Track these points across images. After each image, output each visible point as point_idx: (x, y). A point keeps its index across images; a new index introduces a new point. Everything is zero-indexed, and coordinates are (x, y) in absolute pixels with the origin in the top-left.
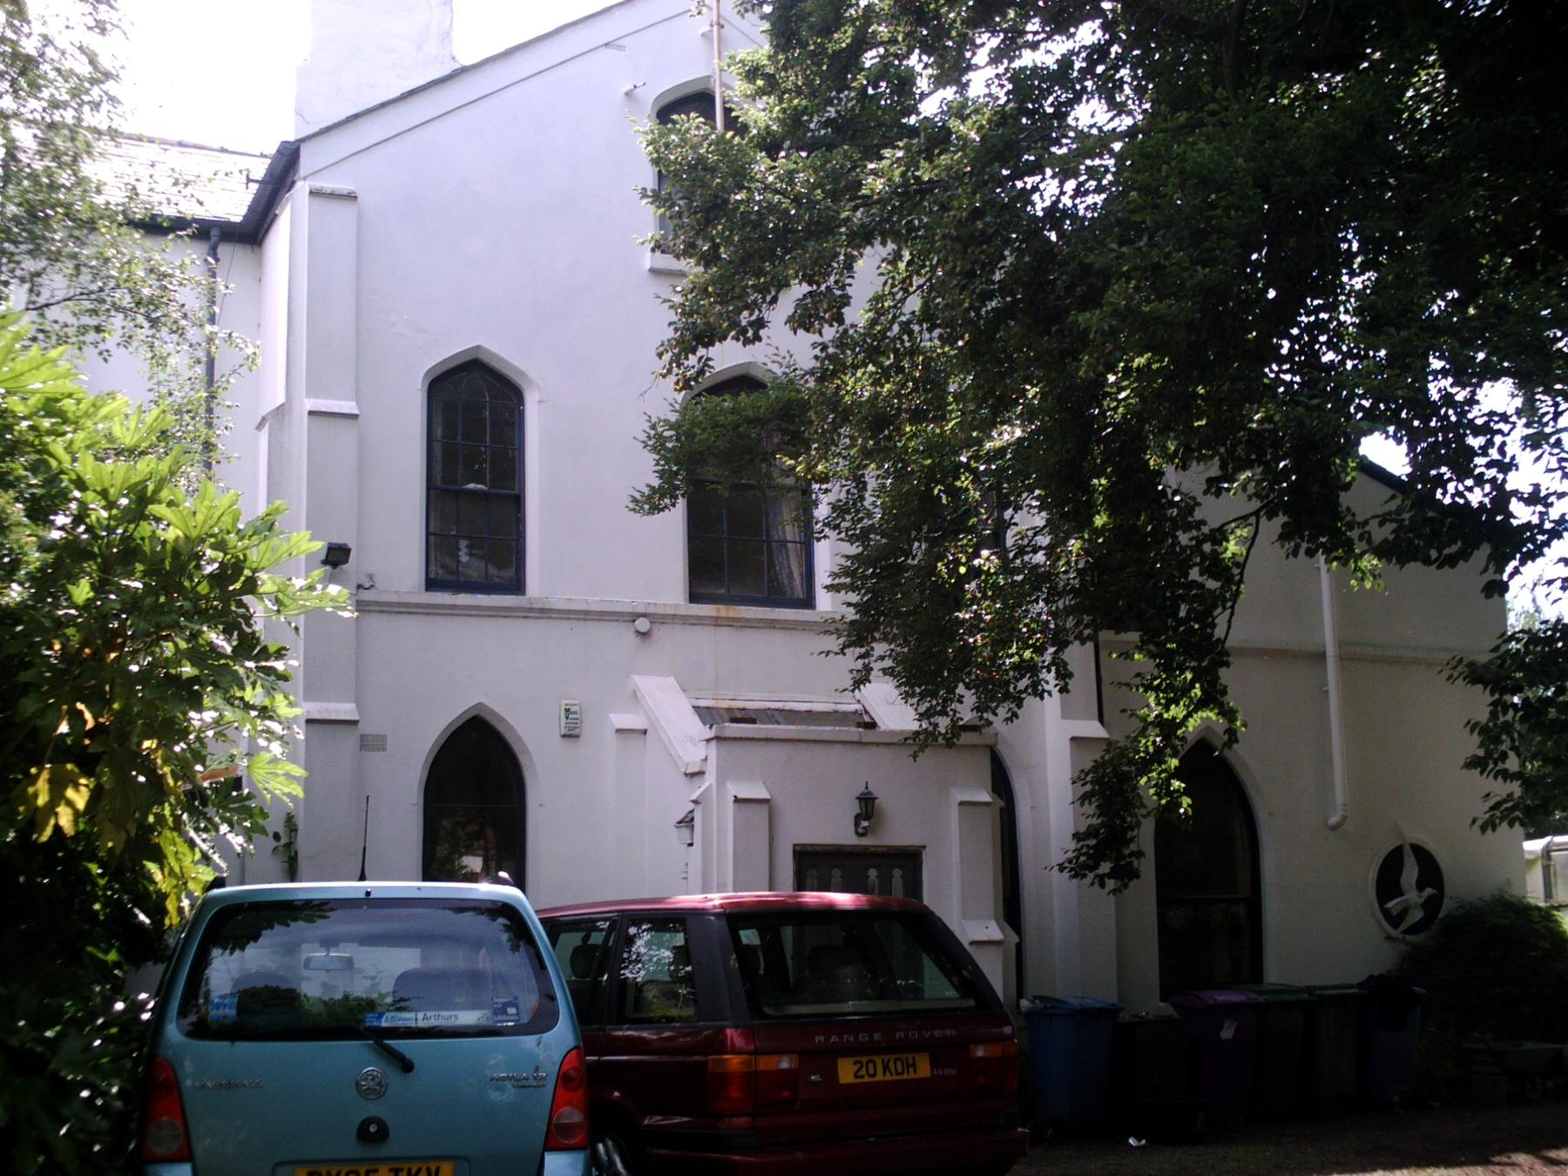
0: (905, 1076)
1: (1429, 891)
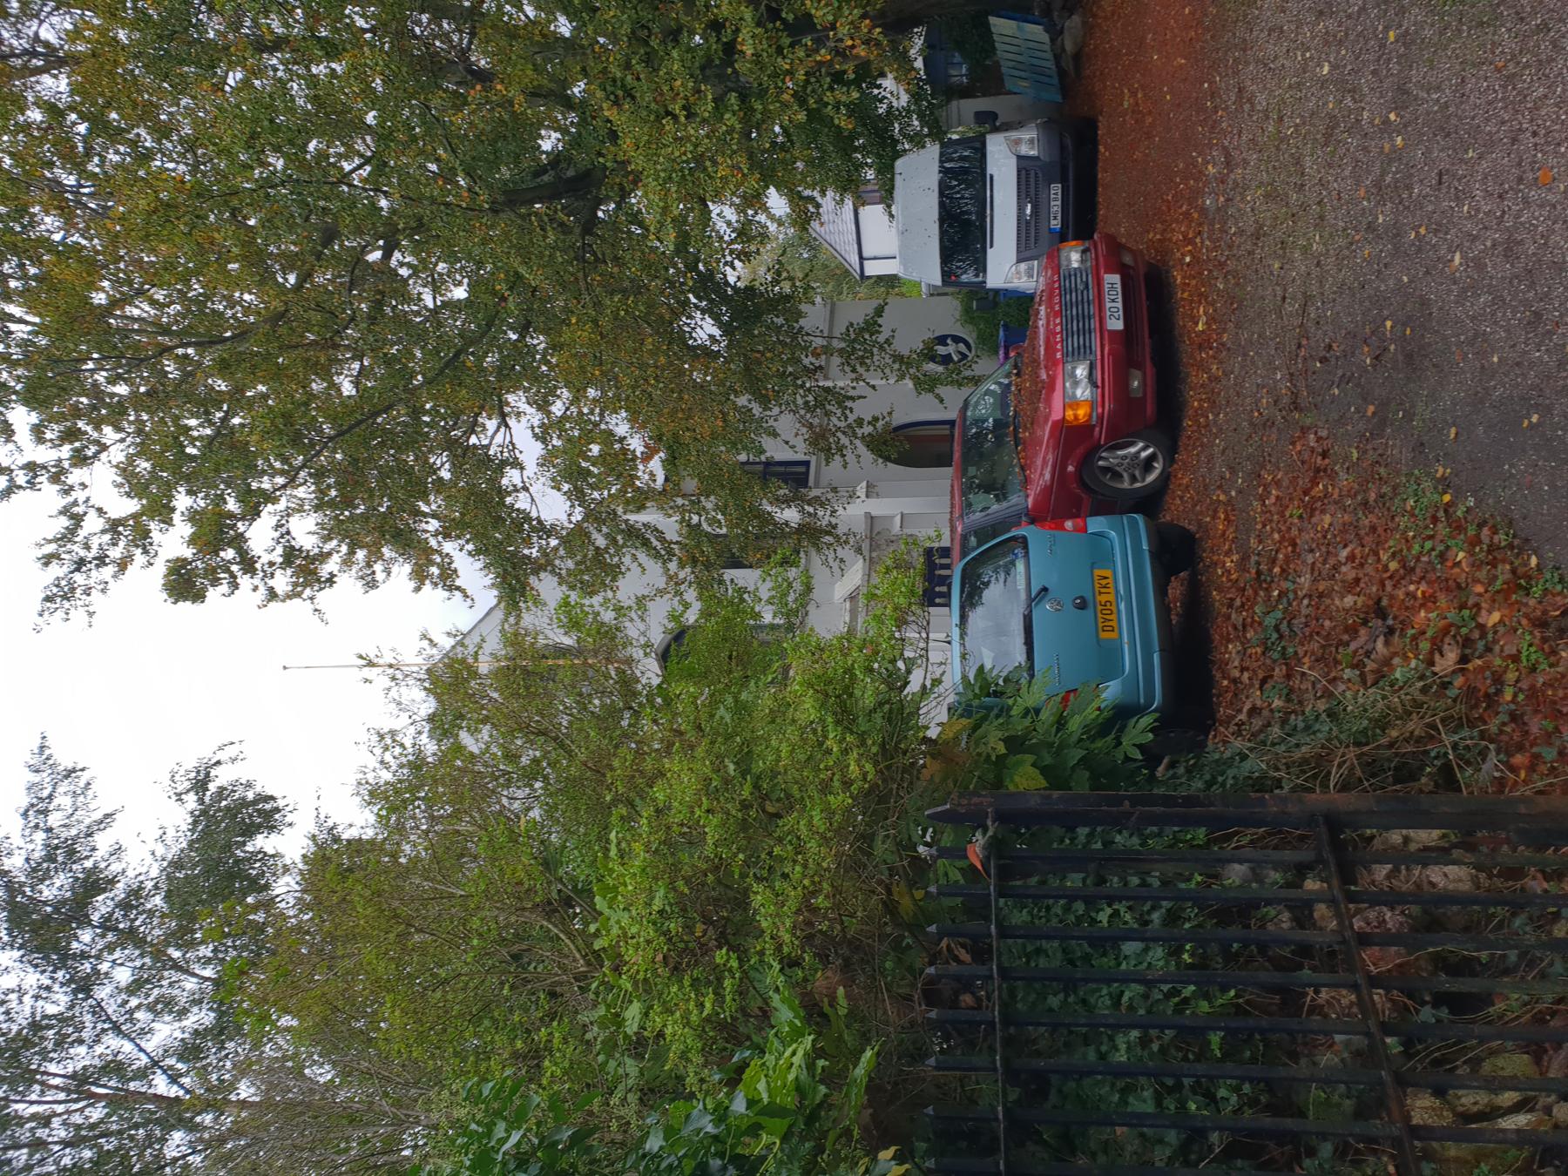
0: (1119, 290)
1: (949, 341)
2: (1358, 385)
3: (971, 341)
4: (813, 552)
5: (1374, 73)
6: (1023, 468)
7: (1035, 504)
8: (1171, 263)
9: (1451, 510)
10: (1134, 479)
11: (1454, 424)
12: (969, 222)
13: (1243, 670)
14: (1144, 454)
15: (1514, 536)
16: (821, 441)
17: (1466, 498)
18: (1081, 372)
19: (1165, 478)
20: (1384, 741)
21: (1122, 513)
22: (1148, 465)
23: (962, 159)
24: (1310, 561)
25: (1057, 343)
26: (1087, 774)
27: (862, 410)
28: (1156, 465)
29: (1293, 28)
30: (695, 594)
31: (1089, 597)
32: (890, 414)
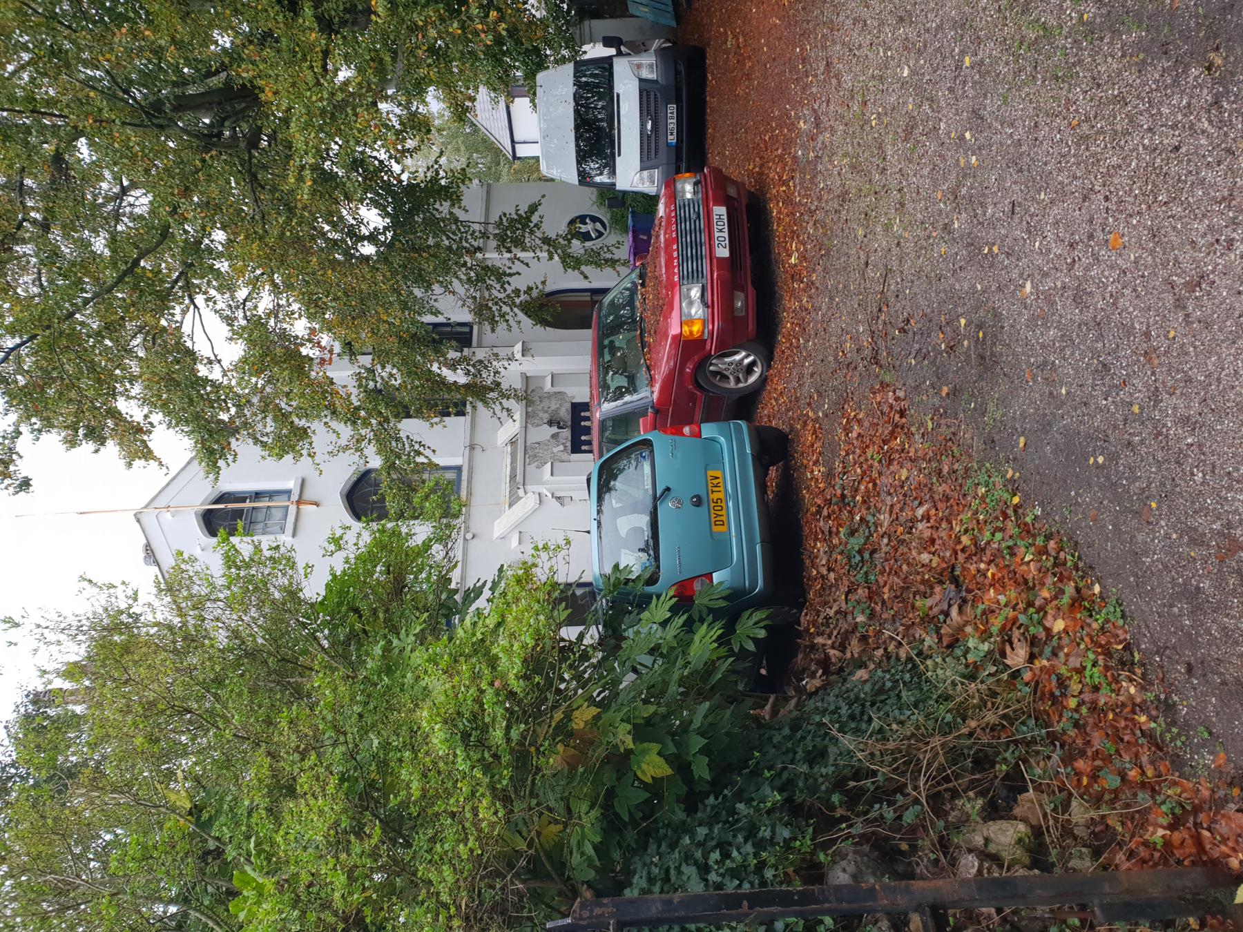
0: (726, 221)
1: (588, 221)
2: (933, 362)
3: (606, 221)
4: (480, 405)
5: (951, 90)
6: (648, 368)
7: (659, 398)
8: (768, 196)
9: (1020, 511)
10: (738, 380)
11: (1023, 434)
12: (600, 129)
13: (829, 570)
14: (746, 361)
15: (1080, 558)
16: (482, 310)
17: (1034, 507)
18: (695, 293)
19: (763, 380)
20: (965, 731)
21: (727, 419)
22: (749, 369)
23: (593, 75)
24: (889, 503)
25: (675, 267)
26: (707, 760)
27: (516, 283)
28: (756, 369)
29: (876, 24)
30: (375, 449)
31: (703, 494)
32: (544, 283)
